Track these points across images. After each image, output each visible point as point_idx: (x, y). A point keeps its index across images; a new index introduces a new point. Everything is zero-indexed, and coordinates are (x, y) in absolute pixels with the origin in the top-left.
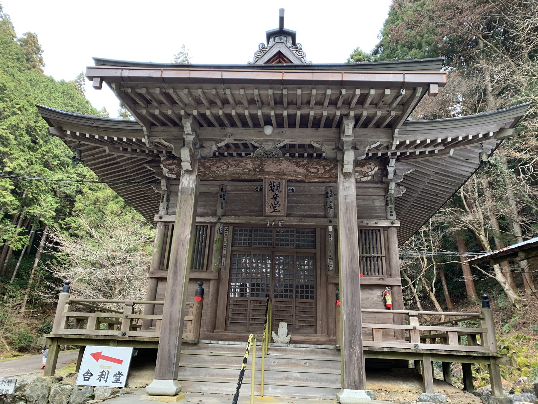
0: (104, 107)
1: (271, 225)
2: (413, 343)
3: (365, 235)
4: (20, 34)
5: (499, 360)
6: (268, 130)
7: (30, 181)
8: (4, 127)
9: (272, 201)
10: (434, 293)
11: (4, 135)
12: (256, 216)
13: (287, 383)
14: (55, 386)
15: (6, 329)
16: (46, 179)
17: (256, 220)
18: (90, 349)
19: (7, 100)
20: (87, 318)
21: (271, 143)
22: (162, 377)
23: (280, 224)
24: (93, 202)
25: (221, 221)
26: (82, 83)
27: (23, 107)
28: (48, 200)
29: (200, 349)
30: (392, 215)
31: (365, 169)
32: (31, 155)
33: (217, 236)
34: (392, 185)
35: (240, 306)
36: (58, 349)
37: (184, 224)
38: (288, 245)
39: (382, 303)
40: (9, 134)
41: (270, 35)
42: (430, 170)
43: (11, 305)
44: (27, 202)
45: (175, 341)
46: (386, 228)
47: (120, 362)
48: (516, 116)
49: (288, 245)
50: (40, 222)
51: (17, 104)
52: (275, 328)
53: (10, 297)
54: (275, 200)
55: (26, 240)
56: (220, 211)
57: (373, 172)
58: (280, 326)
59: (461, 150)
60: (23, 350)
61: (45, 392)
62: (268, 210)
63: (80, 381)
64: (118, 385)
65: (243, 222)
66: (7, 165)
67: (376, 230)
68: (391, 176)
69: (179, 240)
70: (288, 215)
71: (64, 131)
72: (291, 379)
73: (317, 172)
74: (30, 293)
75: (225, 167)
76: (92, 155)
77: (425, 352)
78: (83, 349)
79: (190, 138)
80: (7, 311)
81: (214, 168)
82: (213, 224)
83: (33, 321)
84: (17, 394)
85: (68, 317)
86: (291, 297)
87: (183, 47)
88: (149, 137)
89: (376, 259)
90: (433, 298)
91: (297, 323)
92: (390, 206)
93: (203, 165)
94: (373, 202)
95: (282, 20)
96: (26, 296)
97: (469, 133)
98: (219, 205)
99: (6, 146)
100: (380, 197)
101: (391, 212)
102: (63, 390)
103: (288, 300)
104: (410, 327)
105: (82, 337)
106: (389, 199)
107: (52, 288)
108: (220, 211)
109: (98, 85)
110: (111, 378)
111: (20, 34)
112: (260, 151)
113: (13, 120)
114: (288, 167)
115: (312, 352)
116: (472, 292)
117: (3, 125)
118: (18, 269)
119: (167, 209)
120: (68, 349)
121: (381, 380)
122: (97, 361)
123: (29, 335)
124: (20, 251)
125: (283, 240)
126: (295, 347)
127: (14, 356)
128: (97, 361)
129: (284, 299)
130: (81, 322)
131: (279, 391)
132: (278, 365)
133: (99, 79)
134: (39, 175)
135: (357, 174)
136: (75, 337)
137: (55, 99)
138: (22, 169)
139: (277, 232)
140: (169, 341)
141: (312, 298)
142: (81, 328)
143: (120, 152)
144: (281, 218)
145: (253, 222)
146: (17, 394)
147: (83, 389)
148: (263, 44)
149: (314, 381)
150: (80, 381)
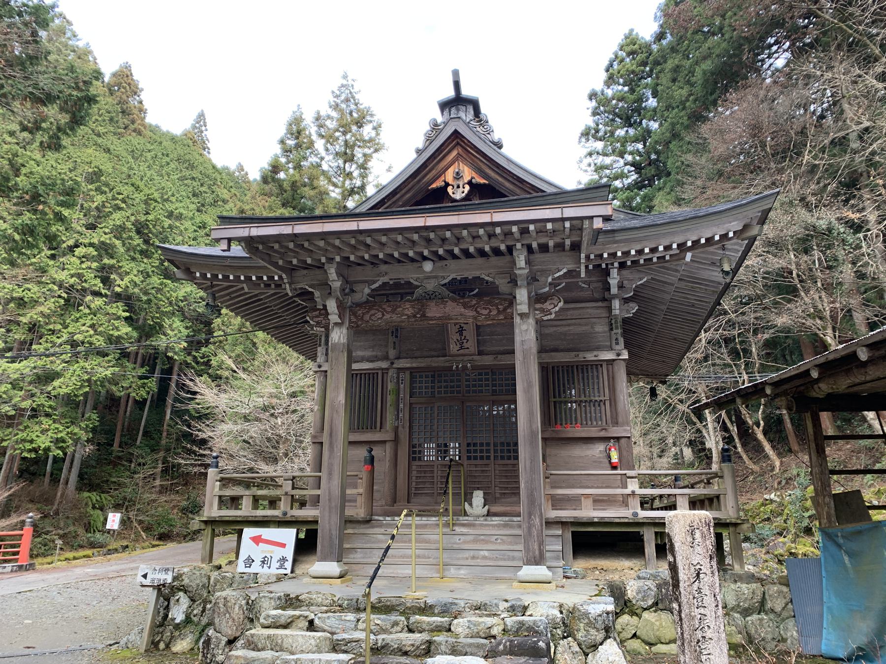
0: (240, 164)
1: (457, 367)
2: (631, 511)
3: (583, 373)
4: (108, 68)
5: (739, 527)
6: (428, 266)
7: (149, 301)
8: (107, 230)
9: (457, 336)
10: (761, 428)
11: (108, 241)
12: (438, 356)
13: (472, 562)
14: (214, 575)
15: (138, 510)
16: (168, 295)
17: (439, 362)
18: (249, 532)
19: (107, 189)
20: (242, 497)
21: (433, 281)
22: (324, 559)
23: (469, 365)
24: (237, 327)
25: (395, 366)
26: (203, 128)
27: (128, 197)
28: (174, 326)
29: (373, 527)
30: (617, 344)
31: (547, 305)
32: (147, 264)
33: (390, 386)
34: (616, 304)
35: (425, 472)
36: (214, 535)
37: (337, 388)
38: (481, 391)
39: (607, 461)
40: (114, 239)
41: (445, 105)
42: (673, 279)
43: (142, 476)
44: (147, 329)
45: (336, 520)
46: (610, 362)
47: (283, 545)
48: (761, 209)
49: (481, 391)
50: (168, 357)
51: (119, 194)
52: (468, 498)
53: (139, 464)
54: (461, 335)
55: (153, 384)
56: (392, 353)
57: (557, 309)
58: (474, 495)
59: (703, 252)
60: (164, 537)
61: (205, 580)
62: (454, 348)
63: (241, 568)
64: (283, 571)
65: (422, 365)
66: (117, 283)
67: (597, 365)
68: (614, 290)
69: (332, 407)
70: (480, 353)
71: (192, 273)
72: (478, 558)
73: (489, 314)
74: (165, 457)
75: (379, 315)
76: (228, 294)
77: (645, 521)
78: (240, 533)
79: (337, 284)
80: (137, 484)
81: (367, 317)
82: (385, 371)
83: (173, 496)
84: (175, 583)
85: (220, 497)
86: (488, 458)
87: (345, 77)
88: (290, 284)
89: (597, 404)
90: (760, 436)
91: (498, 490)
92: (615, 331)
93: (355, 314)
94: (592, 327)
95: (457, 85)
96: (160, 462)
97: (702, 234)
98: (391, 345)
99: (112, 258)
100: (602, 320)
101: (617, 339)
102: (224, 578)
103: (485, 462)
104: (628, 491)
105: (239, 519)
106: (613, 322)
107: (194, 452)
108: (392, 353)
109: (226, 248)
110: (275, 564)
111: (108, 68)
112: (421, 292)
113: (117, 218)
114: (454, 309)
115: (505, 526)
116: (828, 423)
117: (105, 227)
118: (145, 426)
119: (327, 354)
120: (225, 534)
121: (599, 557)
122: (258, 545)
123: (171, 516)
124: (145, 400)
125: (475, 386)
126: (486, 520)
127: (154, 546)
128: (258, 545)
129: (479, 462)
130: (235, 501)
131: (462, 572)
132: (465, 542)
133: (226, 241)
134: (159, 290)
135: (537, 312)
136: (231, 519)
137: (168, 175)
138: (136, 285)
139: (467, 375)
140: (330, 519)
141: (414, 447)
142: (237, 508)
143: (262, 289)
144: (470, 358)
145: (434, 365)
146: (175, 583)
147: (245, 577)
148: (435, 120)
149: (505, 560)
150: (241, 568)
